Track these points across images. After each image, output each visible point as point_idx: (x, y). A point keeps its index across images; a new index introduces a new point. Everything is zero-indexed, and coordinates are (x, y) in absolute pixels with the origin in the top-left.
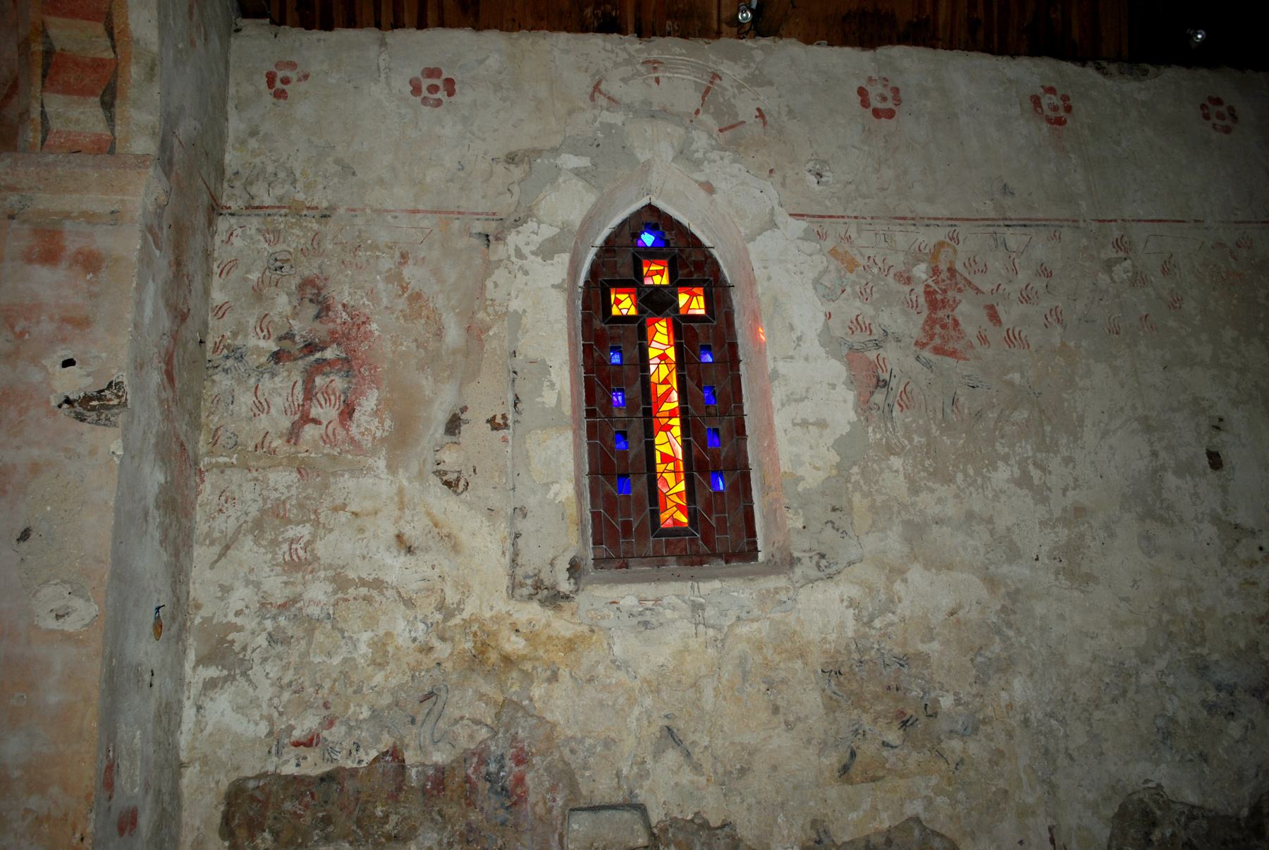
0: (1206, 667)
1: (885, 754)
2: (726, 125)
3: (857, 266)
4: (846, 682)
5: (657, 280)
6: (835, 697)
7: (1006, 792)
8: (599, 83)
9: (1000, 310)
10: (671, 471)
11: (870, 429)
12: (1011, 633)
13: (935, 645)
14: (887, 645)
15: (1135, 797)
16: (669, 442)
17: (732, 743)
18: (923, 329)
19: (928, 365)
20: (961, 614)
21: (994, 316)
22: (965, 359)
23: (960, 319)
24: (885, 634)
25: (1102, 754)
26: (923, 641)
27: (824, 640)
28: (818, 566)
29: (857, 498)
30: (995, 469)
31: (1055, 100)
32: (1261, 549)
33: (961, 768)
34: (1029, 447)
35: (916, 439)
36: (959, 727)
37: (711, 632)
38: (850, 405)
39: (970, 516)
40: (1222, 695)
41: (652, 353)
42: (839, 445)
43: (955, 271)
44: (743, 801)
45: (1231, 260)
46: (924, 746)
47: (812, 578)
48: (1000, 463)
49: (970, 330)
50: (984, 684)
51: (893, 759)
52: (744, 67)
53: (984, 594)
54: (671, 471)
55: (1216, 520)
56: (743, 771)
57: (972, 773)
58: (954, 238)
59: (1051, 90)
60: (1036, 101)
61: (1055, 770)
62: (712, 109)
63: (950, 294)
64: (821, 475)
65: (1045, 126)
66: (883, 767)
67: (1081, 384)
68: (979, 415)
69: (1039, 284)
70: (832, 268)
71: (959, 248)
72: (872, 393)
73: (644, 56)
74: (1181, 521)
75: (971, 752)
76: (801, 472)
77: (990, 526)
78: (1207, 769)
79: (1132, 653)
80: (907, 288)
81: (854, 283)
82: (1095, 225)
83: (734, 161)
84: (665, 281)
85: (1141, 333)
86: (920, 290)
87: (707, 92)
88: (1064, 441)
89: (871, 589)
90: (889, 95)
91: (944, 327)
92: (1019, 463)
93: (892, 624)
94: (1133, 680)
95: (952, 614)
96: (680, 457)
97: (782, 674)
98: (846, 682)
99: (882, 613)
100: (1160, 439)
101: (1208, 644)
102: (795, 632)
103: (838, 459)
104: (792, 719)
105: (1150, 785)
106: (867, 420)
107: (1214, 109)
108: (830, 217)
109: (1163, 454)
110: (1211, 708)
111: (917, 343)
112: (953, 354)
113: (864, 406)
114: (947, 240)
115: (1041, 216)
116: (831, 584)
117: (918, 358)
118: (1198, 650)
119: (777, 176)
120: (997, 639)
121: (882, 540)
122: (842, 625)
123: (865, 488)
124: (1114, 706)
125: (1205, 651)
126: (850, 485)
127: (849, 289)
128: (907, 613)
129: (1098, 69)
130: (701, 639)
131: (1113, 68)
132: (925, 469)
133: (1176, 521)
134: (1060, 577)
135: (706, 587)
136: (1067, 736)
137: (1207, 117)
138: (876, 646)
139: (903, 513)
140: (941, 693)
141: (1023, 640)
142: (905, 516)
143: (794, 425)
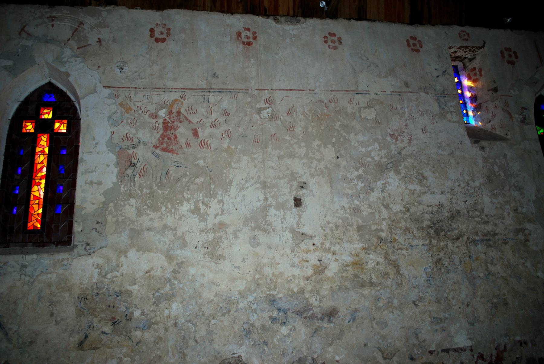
0: (275, 300)
1: (102, 337)
2: (81, 46)
3: (131, 110)
4: (88, 303)
5: (46, 116)
6: (82, 310)
7: (160, 357)
8: (25, 26)
9: (200, 131)
10: (37, 204)
11: (122, 186)
12: (176, 282)
13: (136, 287)
14: (112, 286)
15: (227, 361)
16: (39, 191)
17: (29, 330)
18: (159, 140)
19: (158, 156)
20: (152, 272)
21: (195, 134)
22: (177, 154)
23: (178, 135)
24: (111, 281)
25: (213, 340)
26: (130, 285)
27: (81, 283)
28: (85, 249)
29: (109, 218)
30: (182, 205)
31: (249, 34)
32: (314, 245)
33: (139, 345)
34: (201, 195)
35: (145, 190)
36: (141, 326)
37: (27, 278)
38: (115, 174)
39: (165, 227)
40: (280, 314)
41: (38, 149)
42: (105, 193)
43: (181, 113)
44: (29, 356)
45: (324, 108)
46: (122, 334)
47: (81, 254)
48: (185, 203)
49: (182, 141)
50: (157, 306)
51: (106, 339)
52: (96, 20)
53: (165, 263)
54: (37, 204)
55: (292, 230)
56: (31, 343)
57: (144, 347)
58: (183, 98)
59: (248, 29)
60: (239, 34)
61: (187, 347)
62: (76, 38)
63: (175, 124)
64: (95, 207)
65: (241, 46)
66: (100, 343)
67: (234, 166)
68: (178, 180)
69: (222, 119)
70: (119, 111)
71: (184, 102)
72: (126, 169)
73: (49, 15)
74: (274, 231)
75: (145, 338)
76: (85, 205)
77: (174, 232)
78: (266, 349)
79: (237, 293)
80: (154, 121)
81: (128, 118)
82: (256, 92)
83: (82, 62)
84: (50, 117)
85: (270, 142)
86: (161, 121)
87: (76, 30)
88: (220, 193)
89: (108, 260)
90: (165, 31)
91: (169, 139)
92: (195, 203)
93: (116, 277)
94: (235, 305)
95: (147, 273)
96: (42, 197)
97: (58, 298)
98: (88, 303)
99: (112, 271)
100: (270, 192)
101: (277, 289)
102: (68, 279)
103: (104, 199)
104: (59, 319)
105: (235, 356)
106: (122, 181)
107: (330, 38)
108: (123, 88)
109: (270, 199)
110: (273, 320)
111: (154, 146)
112: (171, 151)
113: (121, 175)
114: (180, 98)
115: (229, 87)
116: (90, 257)
117: (153, 153)
118: (272, 292)
119: (101, 69)
120: (168, 285)
121: (118, 238)
122: (91, 277)
123: (115, 213)
124: (223, 318)
125: (275, 293)
126: (107, 212)
127: (125, 121)
128: (125, 272)
129: (275, 20)
130: (22, 281)
131: (283, 19)
132: (147, 205)
133: (271, 230)
134: (206, 256)
135: (29, 258)
136: (196, 331)
137: (326, 42)
138: (106, 287)
139: (131, 225)
140: (135, 309)
141: (181, 286)
142: (132, 226)
143: (86, 183)
